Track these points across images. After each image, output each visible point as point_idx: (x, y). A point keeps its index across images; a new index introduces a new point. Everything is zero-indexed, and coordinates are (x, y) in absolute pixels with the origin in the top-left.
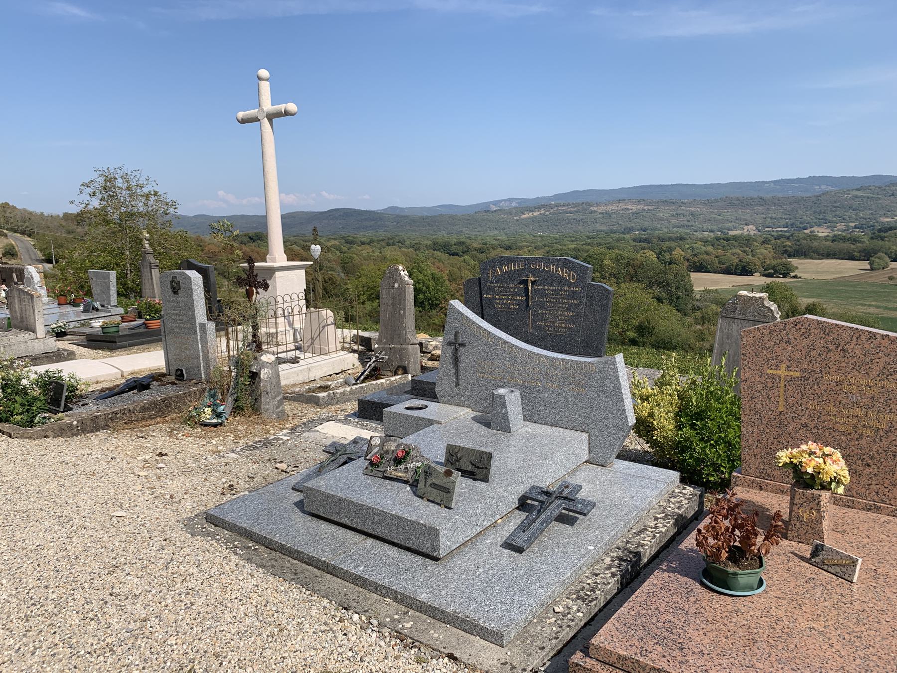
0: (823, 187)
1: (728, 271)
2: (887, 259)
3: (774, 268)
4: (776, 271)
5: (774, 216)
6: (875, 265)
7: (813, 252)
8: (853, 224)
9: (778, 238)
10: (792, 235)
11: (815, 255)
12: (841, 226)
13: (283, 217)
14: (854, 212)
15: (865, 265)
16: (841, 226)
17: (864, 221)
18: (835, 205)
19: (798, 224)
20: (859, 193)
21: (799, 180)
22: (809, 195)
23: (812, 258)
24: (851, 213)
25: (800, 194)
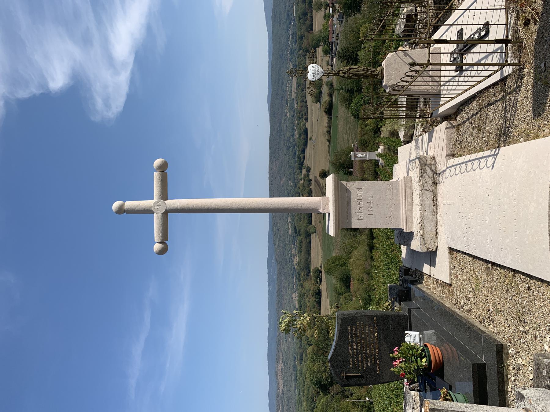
0: (273, 261)
2: (310, 226)
3: (316, 278)
4: (318, 277)
5: (287, 284)
8: (293, 246)
9: (300, 280)
11: (309, 260)
12: (293, 251)
13: (271, 196)
15: (313, 236)
16: (293, 251)
22: (276, 268)
24: (287, 247)
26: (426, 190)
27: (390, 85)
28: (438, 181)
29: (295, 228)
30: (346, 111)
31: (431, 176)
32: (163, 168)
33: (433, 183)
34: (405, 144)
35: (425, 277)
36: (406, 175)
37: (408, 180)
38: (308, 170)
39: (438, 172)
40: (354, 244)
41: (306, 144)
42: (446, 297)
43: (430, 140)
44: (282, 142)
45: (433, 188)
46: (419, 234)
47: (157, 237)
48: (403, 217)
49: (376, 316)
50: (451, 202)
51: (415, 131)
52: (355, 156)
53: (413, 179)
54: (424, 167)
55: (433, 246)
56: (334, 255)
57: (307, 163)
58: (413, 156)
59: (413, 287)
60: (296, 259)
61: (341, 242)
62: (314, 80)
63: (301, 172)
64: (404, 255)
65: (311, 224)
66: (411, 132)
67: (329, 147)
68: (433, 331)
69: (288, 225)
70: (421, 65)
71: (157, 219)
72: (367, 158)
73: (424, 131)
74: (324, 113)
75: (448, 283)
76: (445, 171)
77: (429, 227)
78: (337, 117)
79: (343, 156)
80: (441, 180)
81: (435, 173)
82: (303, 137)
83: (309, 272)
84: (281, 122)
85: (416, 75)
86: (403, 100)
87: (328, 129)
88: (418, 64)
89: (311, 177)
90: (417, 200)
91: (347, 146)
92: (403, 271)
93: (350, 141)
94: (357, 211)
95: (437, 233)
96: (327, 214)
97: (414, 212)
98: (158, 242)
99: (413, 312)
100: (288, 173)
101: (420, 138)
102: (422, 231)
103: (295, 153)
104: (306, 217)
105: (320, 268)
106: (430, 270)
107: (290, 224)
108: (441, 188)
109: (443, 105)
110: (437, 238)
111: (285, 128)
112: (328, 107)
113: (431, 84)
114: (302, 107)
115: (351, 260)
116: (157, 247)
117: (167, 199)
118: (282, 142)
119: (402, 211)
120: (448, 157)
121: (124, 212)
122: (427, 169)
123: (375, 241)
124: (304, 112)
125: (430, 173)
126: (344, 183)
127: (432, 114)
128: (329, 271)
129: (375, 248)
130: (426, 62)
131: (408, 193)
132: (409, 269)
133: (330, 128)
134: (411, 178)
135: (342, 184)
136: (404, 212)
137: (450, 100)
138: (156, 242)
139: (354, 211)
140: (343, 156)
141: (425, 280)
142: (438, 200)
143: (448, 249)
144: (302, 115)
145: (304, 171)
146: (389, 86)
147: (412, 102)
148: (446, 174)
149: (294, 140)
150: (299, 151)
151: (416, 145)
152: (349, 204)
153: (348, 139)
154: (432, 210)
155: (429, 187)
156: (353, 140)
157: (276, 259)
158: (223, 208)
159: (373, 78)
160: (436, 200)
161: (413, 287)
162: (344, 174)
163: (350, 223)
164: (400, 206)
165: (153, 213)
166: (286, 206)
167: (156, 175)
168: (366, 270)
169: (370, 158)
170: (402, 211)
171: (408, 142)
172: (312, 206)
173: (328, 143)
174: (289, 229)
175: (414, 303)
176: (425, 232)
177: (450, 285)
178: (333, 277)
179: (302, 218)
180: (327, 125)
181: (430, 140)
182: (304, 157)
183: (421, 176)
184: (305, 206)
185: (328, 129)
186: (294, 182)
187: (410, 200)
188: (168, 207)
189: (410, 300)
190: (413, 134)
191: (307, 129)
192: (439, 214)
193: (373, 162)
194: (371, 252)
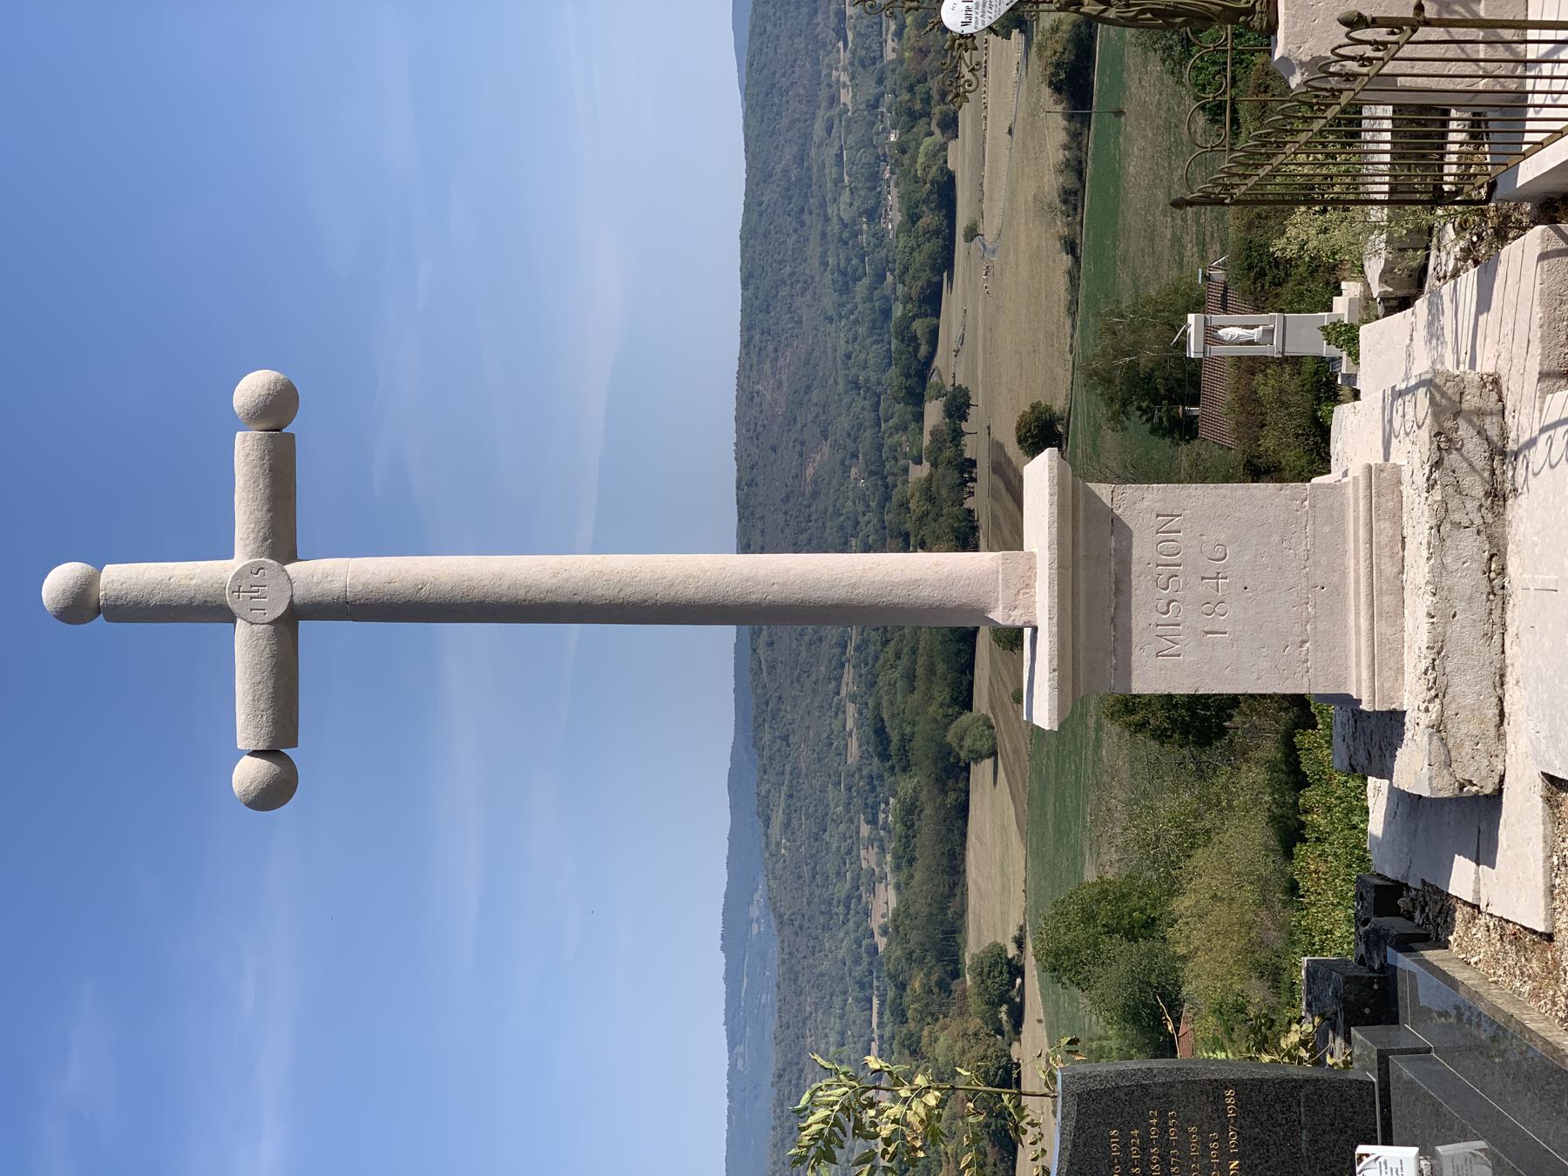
0: (755, 912)
1: (969, 667)
2: (966, 718)
3: (994, 1005)
4: (1003, 998)
5: (833, 1038)
6: (984, 746)
7: (944, 909)
8: (865, 830)
9: (901, 1016)
10: (893, 977)
11: (954, 906)
12: (868, 858)
13: (745, 547)
14: (831, 827)
15: (981, 772)
16: (868, 858)
17: (858, 801)
18: (807, 877)
19: (858, 971)
20: (778, 819)
21: (732, 978)
22: (774, 949)
23: (962, 913)
24: (832, 838)
25: (772, 972)
26: (1457, 525)
27: (1306, 59)
28: (1508, 486)
29: (880, 731)
30: (1169, 80)
31: (1480, 463)
32: (277, 412)
33: (1487, 495)
34: (1389, 311)
35: (1458, 916)
36: (1378, 459)
37: (1383, 481)
38: (959, 406)
39: (1511, 446)
40: (1198, 816)
41: (945, 262)
42: (1535, 995)
43: (1484, 304)
44: (813, 249)
45: (1489, 518)
46: (1425, 720)
47: (247, 727)
48: (1357, 645)
49: (1235, 1084)
50: (1549, 578)
51: (1433, 253)
52: (1210, 336)
53: (1406, 476)
54: (1448, 424)
55: (1484, 772)
56: (1090, 875)
57: (948, 368)
58: (1421, 367)
59: (1403, 962)
60: (885, 901)
61: (1128, 803)
62: (968, 30)
63: (919, 417)
64: (1376, 825)
65: (967, 705)
66: (1413, 259)
67: (1073, 278)
68: (1482, 1144)
69: (840, 710)
70: (1394, 24)
71: (246, 646)
72: (1273, 350)
73: (1469, 253)
74: (1046, 91)
75: (1541, 929)
76: (1532, 442)
77: (1468, 690)
78: (1119, 113)
79: (1149, 334)
80: (1520, 480)
81: (1500, 452)
82: (929, 219)
83: (956, 974)
84: (806, 137)
85: (1380, 54)
86: (1380, 121)
87: (1071, 182)
88: (1375, 23)
89: (974, 447)
90: (1418, 570)
91: (1170, 274)
92: (1370, 897)
93: (1191, 250)
94: (1156, 617)
95: (1502, 714)
96: (1027, 632)
97: (1408, 623)
98: (254, 753)
99: (1402, 1068)
100: (845, 422)
101: (1446, 289)
102: (1435, 708)
103: (887, 313)
104: (941, 668)
105: (1012, 951)
106: (1477, 880)
107: (851, 709)
108: (1523, 516)
109: (1541, 145)
110: (1501, 737)
111: (831, 172)
112: (1069, 57)
113: (1482, 51)
114: (923, 52)
115: (1182, 904)
116: (248, 772)
117: (293, 558)
118: (813, 249)
119: (1356, 619)
120: (1548, 383)
121: (98, 610)
122: (1465, 431)
123: (1310, 796)
124: (934, 84)
125: (1475, 449)
126: (1103, 490)
127: (1492, 187)
128: (1065, 965)
129: (1311, 835)
130: (1410, 13)
131: (1384, 539)
132: (1398, 888)
133: (1080, 173)
134: (1397, 469)
135: (1093, 497)
136: (1364, 625)
137: (1550, 141)
138: (241, 754)
139: (1141, 620)
140: (1149, 334)
141: (1459, 928)
142: (1510, 570)
143: (1539, 783)
144: (927, 101)
145: (934, 413)
146: (1302, 64)
147: (1418, 123)
148: (1537, 456)
149: (880, 237)
150: (908, 299)
151: (1430, 324)
152: (1122, 586)
153: (1176, 241)
154: (1483, 613)
155: (1470, 511)
156: (1202, 244)
157: (773, 904)
158: (551, 598)
159: (1234, 22)
160: (1502, 571)
161: (1403, 962)
162: (1153, 431)
163: (1125, 669)
164: (1346, 595)
165: (232, 619)
166: (837, 594)
167: (246, 447)
168: (1262, 955)
169: (1291, 350)
170: (1356, 619)
171: (1404, 303)
172: (957, 596)
173: (1067, 260)
174: (844, 733)
175: (1411, 1032)
176: (1449, 713)
177: (1549, 937)
178: (1083, 1000)
179: (920, 671)
180: (1061, 156)
181: (1484, 304)
182: (934, 334)
183: (1437, 464)
184: (926, 595)
185: (1071, 182)
186: (876, 472)
187: (1389, 569)
188: (300, 594)
189: (1394, 1019)
190: (1424, 268)
191: (951, 178)
192: (1511, 631)
193: (1309, 368)
194: (1289, 855)
